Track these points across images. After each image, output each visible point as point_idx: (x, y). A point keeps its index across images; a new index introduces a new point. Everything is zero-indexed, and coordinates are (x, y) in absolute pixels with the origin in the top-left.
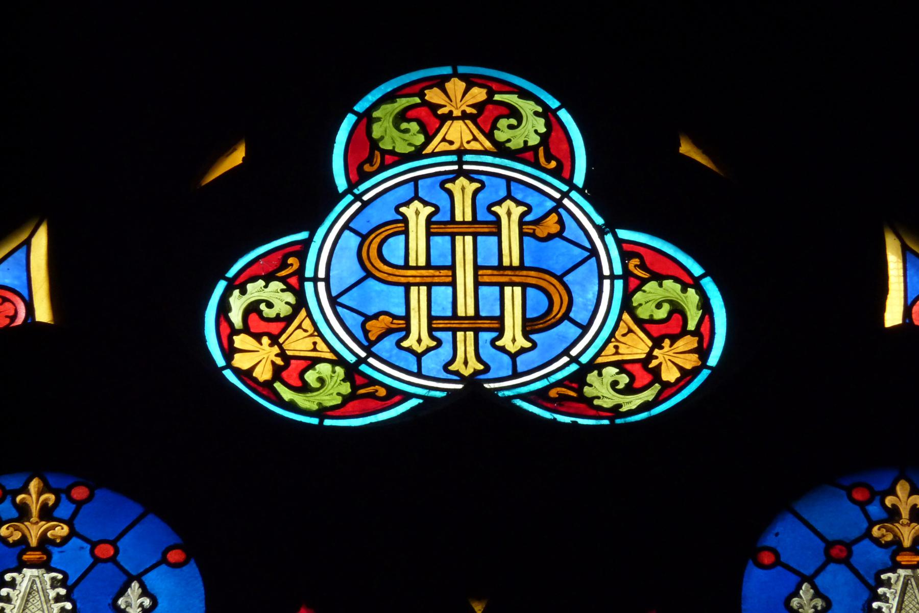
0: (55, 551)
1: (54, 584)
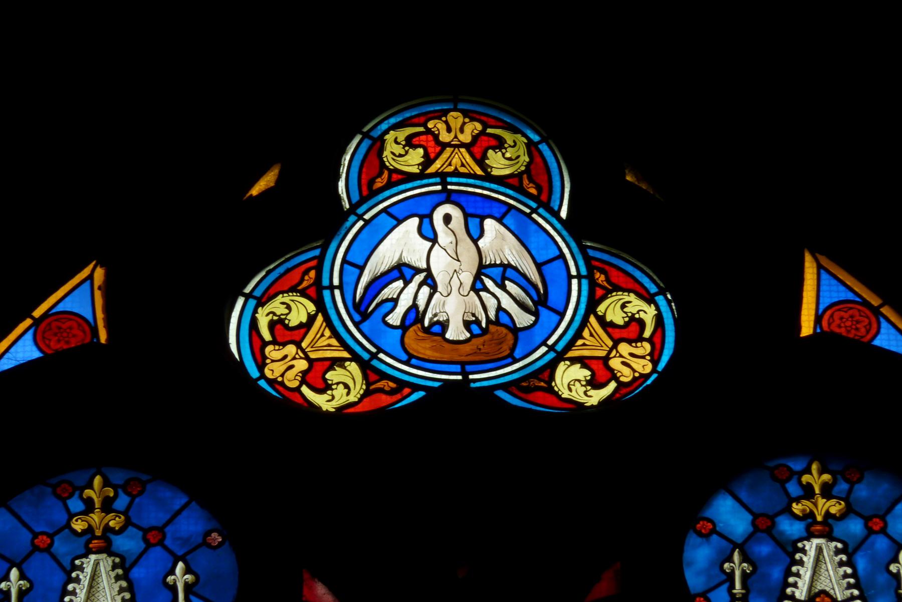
1: (114, 567)
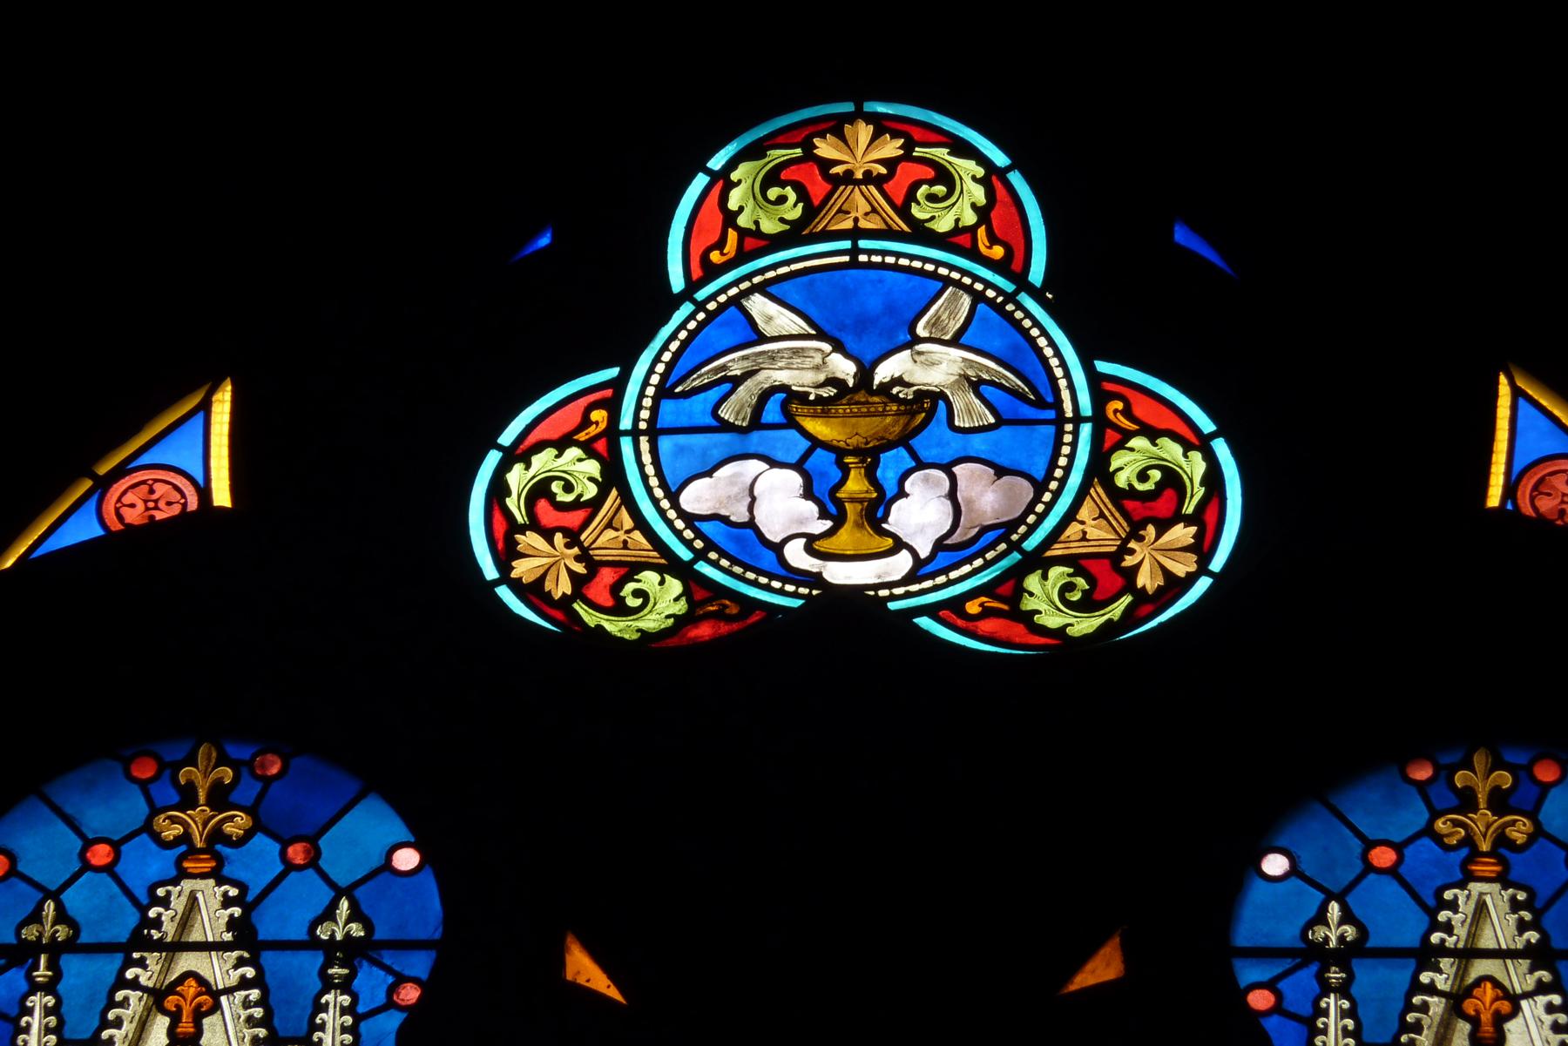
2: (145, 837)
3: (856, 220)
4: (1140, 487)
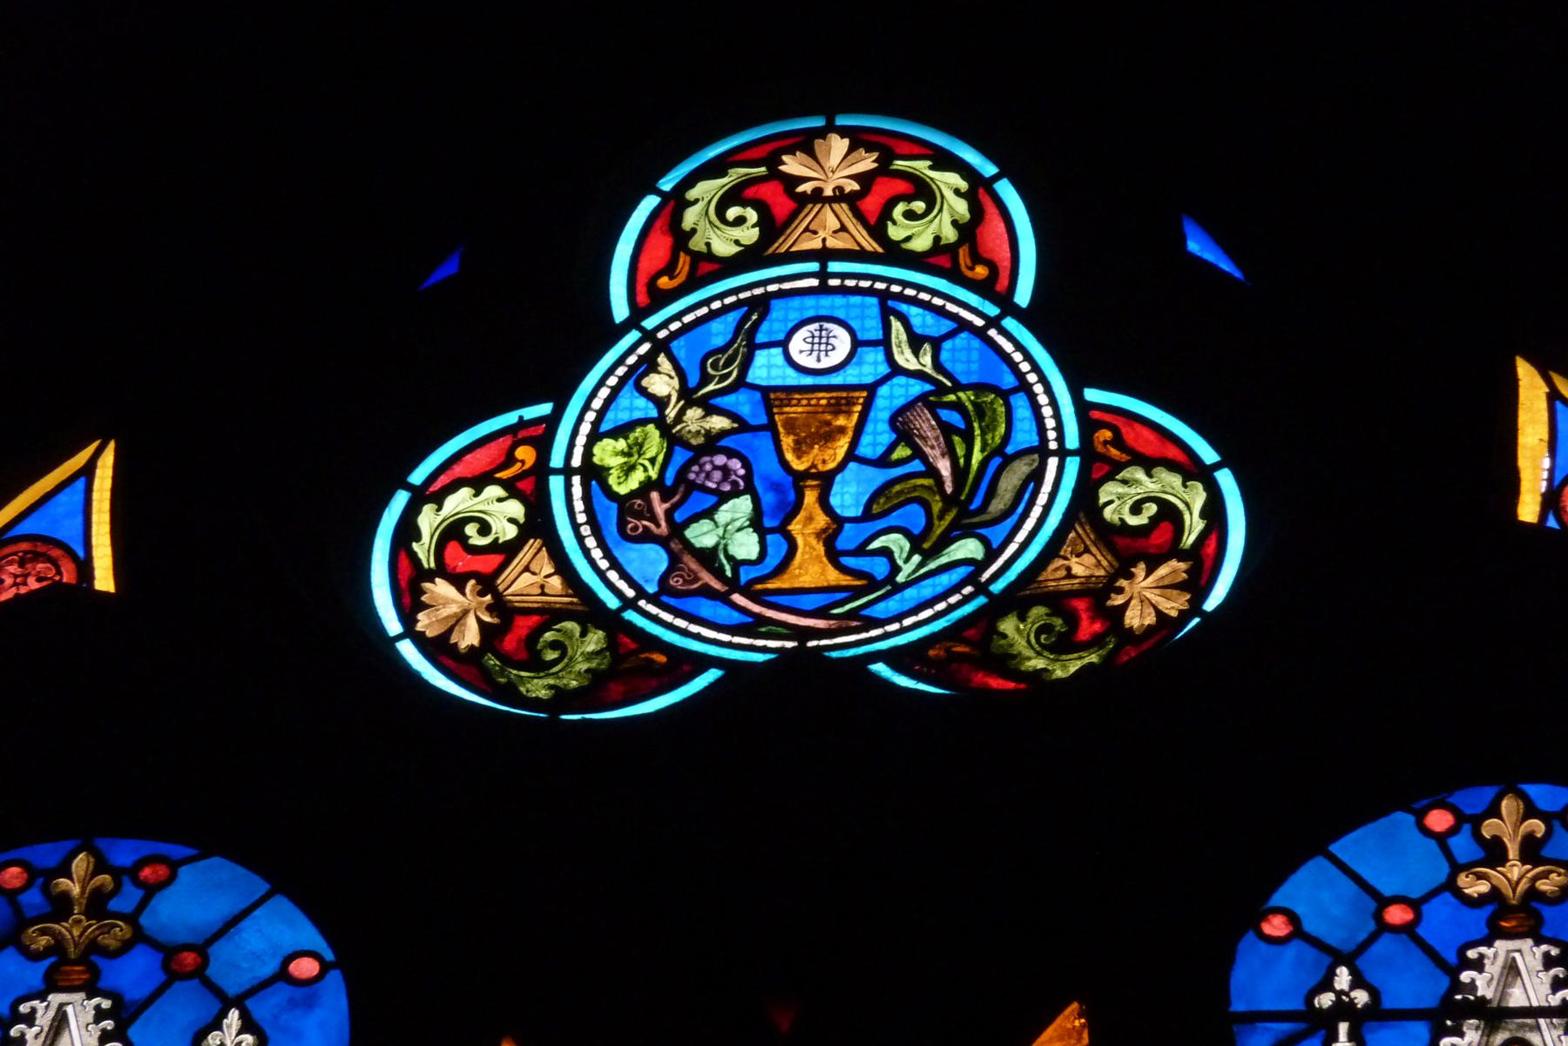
0: (1548, 912)
1: (100, 1015)
2: (1447, 896)
3: (824, 240)
4: (1133, 521)
